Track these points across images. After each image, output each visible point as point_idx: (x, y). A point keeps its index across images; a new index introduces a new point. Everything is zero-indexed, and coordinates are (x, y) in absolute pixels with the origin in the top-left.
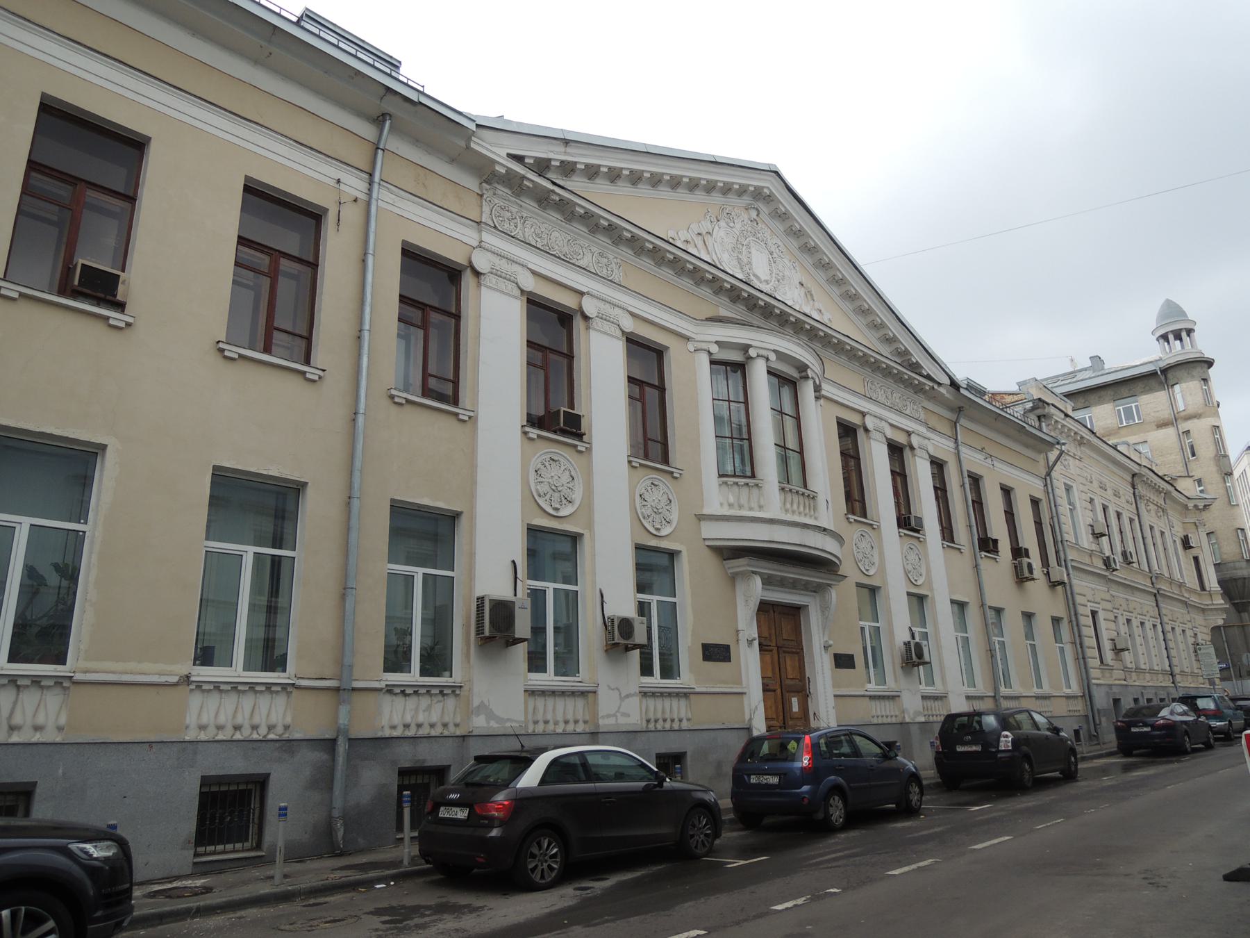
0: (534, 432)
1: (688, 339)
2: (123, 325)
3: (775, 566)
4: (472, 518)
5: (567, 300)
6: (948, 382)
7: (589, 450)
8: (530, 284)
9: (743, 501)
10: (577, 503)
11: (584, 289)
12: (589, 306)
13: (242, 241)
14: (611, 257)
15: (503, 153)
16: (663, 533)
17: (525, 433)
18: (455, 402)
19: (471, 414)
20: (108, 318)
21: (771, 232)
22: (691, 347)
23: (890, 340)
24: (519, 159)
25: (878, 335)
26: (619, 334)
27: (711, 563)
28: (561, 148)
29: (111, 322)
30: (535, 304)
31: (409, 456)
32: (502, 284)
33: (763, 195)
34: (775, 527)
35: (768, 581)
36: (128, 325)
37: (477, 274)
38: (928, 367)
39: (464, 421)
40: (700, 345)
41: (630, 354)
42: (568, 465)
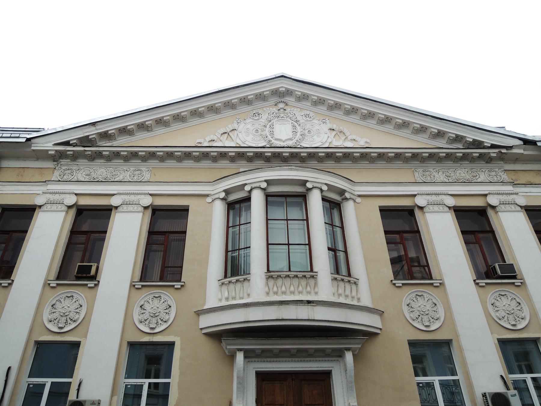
0: (482, 282)
1: (207, 196)
2: (439, 285)
3: (252, 341)
4: (458, 341)
6: (521, 143)
8: (451, 202)
10: (442, 319)
11: (416, 193)
13: (386, 232)
14: (431, 170)
15: (51, 144)
16: (519, 327)
17: (477, 284)
19: (441, 282)
20: (174, 286)
21: (298, 111)
22: (209, 200)
23: (440, 134)
24: (67, 143)
25: (427, 136)
26: (519, 209)
29: (175, 287)
30: (460, 212)
31: (405, 314)
32: (508, 207)
33: (282, 92)
34: (283, 307)
35: (249, 355)
36: (182, 286)
37: (493, 207)
38: (488, 140)
40: (214, 197)
42: (430, 297)
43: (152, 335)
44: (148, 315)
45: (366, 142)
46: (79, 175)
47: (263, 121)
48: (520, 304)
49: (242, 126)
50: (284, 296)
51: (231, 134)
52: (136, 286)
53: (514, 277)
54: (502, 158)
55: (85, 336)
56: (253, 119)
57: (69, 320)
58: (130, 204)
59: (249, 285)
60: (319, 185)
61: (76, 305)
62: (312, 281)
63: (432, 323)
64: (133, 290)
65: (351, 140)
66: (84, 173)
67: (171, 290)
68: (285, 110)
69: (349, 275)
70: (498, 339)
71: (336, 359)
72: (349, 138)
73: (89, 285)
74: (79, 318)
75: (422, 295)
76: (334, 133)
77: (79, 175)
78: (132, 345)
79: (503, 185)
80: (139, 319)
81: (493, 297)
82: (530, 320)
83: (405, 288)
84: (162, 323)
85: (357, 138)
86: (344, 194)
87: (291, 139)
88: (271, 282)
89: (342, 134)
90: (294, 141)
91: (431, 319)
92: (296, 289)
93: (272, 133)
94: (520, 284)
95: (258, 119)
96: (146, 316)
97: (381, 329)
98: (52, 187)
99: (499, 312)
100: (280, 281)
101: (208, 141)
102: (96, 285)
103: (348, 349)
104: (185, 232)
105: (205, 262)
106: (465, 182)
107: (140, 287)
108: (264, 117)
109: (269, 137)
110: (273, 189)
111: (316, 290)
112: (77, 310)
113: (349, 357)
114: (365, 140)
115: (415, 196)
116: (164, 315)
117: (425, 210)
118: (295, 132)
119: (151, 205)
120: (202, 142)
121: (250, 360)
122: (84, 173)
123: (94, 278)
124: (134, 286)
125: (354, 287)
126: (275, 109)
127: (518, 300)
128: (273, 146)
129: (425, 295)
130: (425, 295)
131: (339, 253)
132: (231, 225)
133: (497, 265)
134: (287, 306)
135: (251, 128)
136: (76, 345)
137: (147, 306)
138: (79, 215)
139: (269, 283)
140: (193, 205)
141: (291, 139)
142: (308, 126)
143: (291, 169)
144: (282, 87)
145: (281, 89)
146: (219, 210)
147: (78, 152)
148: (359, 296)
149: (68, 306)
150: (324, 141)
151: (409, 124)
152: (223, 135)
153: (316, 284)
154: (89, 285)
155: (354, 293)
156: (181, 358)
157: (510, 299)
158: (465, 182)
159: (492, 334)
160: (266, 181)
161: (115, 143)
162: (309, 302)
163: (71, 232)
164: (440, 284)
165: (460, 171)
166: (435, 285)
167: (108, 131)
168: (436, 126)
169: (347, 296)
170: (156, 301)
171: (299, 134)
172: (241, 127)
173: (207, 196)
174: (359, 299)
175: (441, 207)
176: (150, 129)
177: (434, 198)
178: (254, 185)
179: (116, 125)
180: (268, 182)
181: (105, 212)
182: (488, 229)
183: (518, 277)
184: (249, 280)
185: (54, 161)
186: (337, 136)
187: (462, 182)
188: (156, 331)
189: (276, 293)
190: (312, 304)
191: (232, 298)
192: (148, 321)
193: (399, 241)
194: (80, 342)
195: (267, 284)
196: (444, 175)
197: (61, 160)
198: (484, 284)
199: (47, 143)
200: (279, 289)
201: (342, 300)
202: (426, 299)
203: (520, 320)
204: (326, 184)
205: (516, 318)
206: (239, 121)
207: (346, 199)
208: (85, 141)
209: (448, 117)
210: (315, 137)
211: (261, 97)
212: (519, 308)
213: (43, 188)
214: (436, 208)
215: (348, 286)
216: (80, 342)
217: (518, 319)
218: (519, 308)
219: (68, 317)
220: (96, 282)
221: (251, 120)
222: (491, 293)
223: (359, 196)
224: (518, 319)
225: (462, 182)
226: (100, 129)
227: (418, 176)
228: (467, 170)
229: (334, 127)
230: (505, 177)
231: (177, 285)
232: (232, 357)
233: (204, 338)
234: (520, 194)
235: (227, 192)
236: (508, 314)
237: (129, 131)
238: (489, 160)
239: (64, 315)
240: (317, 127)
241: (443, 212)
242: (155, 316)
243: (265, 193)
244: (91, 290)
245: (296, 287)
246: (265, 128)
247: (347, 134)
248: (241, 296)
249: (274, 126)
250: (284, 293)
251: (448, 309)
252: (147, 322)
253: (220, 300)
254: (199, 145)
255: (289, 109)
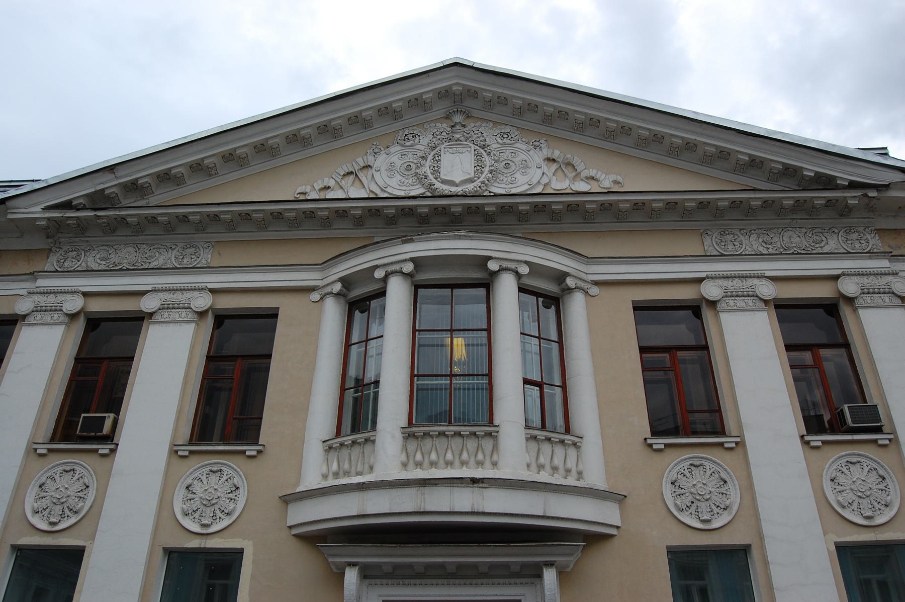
0: (816, 440)
1: (312, 289)
2: (733, 445)
4: (762, 547)
5: (822, 291)
7: (741, 444)
8: (768, 290)
9: (558, 461)
10: (735, 508)
12: (849, 287)
15: (38, 209)
16: (880, 520)
18: (722, 432)
19: (738, 440)
22: (315, 296)
24: (67, 205)
27: (300, 563)
28: (109, 176)
29: (247, 453)
32: (877, 299)
33: (462, 96)
34: (427, 490)
35: (368, 574)
36: (259, 452)
37: (850, 300)
38: (844, 174)
39: (731, 449)
41: (781, 320)
43: (205, 537)
44: (199, 502)
45: (616, 182)
46: (90, 259)
47: (422, 148)
48: (884, 478)
49: (382, 157)
50: (433, 469)
51: (361, 175)
52: (180, 453)
53: (878, 430)
54: (870, 207)
55: (93, 537)
56: (402, 145)
57: (67, 511)
58: (173, 308)
59: (374, 450)
60: (512, 265)
61: (78, 486)
62: (488, 444)
63: (716, 516)
64: (175, 461)
65: (587, 178)
66: (98, 256)
67: (240, 459)
68: (464, 126)
69: (568, 431)
70: (836, 543)
71: (529, 580)
72: (583, 174)
73: (100, 452)
74: (82, 507)
75: (701, 465)
76: (554, 167)
77: (90, 259)
78: (171, 554)
79: (870, 258)
80: (183, 509)
81: (834, 467)
82: (899, 508)
83: (670, 454)
84: (223, 517)
85: (600, 175)
86: (564, 280)
87: (471, 181)
88: (412, 445)
89: (570, 168)
90: (478, 183)
91: (714, 507)
92: (457, 457)
93: (436, 172)
94: (887, 442)
95: (412, 145)
96: (196, 504)
97: (618, 527)
98: (44, 283)
99: (844, 494)
100: (428, 443)
101: (317, 188)
102: (113, 451)
103: (550, 564)
104: (269, 356)
105: (303, 409)
106: (799, 254)
107: (186, 453)
108: (425, 140)
109: (431, 177)
110: (423, 277)
111: (495, 458)
112: (80, 494)
113: (550, 576)
114: (613, 177)
115: (700, 281)
116: (233, 503)
117: (719, 306)
118: (479, 167)
119: (210, 308)
120: (308, 190)
121: (373, 581)
122: (98, 256)
123: (109, 438)
124: (176, 452)
125: (572, 452)
126: (445, 126)
127: (881, 472)
128: (437, 194)
129: (707, 464)
130: (707, 464)
131: (550, 388)
132: (355, 338)
133: (846, 407)
134: (435, 488)
135: (399, 163)
136: (75, 556)
137: (197, 487)
138: (93, 330)
139: (409, 447)
140: (286, 306)
141: (471, 181)
142: (507, 154)
143: (459, 237)
144: (457, 84)
145: (454, 88)
146: (332, 314)
147: (86, 219)
148: (581, 467)
149: (67, 486)
150: (535, 181)
151: (695, 145)
152: (347, 178)
153: (495, 448)
154: (100, 452)
155: (571, 464)
156: (253, 577)
157: (866, 469)
158: (799, 254)
159: (825, 535)
160: (412, 260)
161: (153, 201)
162: (474, 481)
163: (76, 359)
164: (737, 443)
165: (791, 233)
166: (726, 445)
167: (137, 179)
168: (746, 150)
169: (555, 469)
170: (214, 478)
171: (486, 170)
172: (381, 161)
173: (312, 289)
174: (580, 473)
175: (750, 301)
176: (213, 172)
177: (737, 284)
178: (390, 269)
179: (151, 167)
180: (417, 262)
181: (136, 321)
182: (841, 341)
183: (885, 429)
184: (374, 441)
185: (48, 237)
186: (560, 172)
187: (793, 254)
188: (211, 530)
189: (419, 465)
190: (481, 485)
191: (345, 474)
192: (198, 512)
193: (668, 364)
194: (85, 547)
195: (405, 448)
196: (761, 240)
197: (60, 235)
198: (820, 444)
199: (32, 206)
200: (411, 458)
201: (544, 477)
202: (709, 472)
203: (883, 508)
204: (526, 262)
205: (875, 504)
206: (376, 150)
207: (569, 290)
208: (98, 200)
209: (767, 130)
210: (518, 175)
211: (418, 104)
212: (882, 486)
213: (27, 286)
214: (740, 302)
215: (559, 451)
216: (85, 547)
217: (877, 506)
218: (882, 486)
219: (65, 506)
220: (112, 446)
221: (399, 148)
222: (833, 459)
223: (596, 283)
224: (877, 506)
225: (793, 254)
226: (121, 177)
227: (710, 245)
228: (804, 230)
229: (556, 154)
230: (875, 242)
231: (251, 450)
232: (340, 576)
233: (294, 540)
234: (901, 274)
235: (347, 282)
236: (860, 497)
237: (175, 176)
238: (843, 211)
239: (58, 502)
240: (522, 156)
241: (752, 310)
242: (209, 504)
243: (412, 283)
244: (103, 460)
245: (457, 453)
246: (423, 162)
247: (579, 169)
248: (359, 469)
249: (442, 158)
250: (433, 464)
251: (749, 488)
252: (197, 515)
253: (325, 477)
254: (302, 197)
255: (472, 125)
